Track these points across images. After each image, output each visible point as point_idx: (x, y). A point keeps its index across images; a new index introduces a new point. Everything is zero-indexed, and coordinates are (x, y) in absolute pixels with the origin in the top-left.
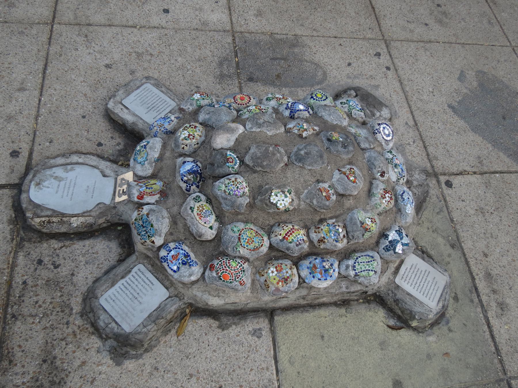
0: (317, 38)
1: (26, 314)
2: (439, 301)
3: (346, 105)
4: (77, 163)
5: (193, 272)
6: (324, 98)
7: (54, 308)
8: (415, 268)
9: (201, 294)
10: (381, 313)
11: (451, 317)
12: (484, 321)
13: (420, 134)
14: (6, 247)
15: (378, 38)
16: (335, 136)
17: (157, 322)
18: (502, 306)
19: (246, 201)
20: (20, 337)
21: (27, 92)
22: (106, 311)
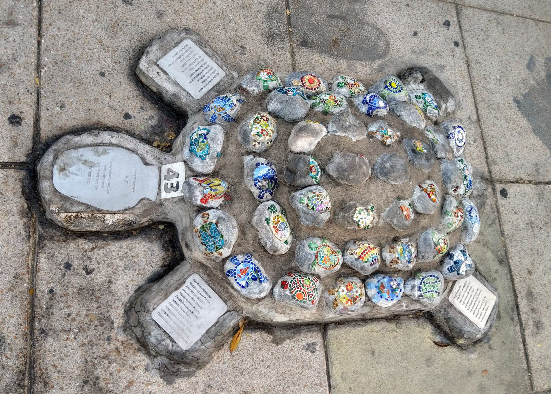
2: (487, 321)
3: (421, 100)
4: (110, 145)
5: (263, 288)
6: (399, 89)
7: (90, 321)
8: (468, 286)
9: (267, 311)
11: (492, 335)
12: (521, 340)
14: (25, 247)
16: (420, 146)
18: (538, 325)
19: (325, 216)
21: (20, 28)
22: (159, 326)
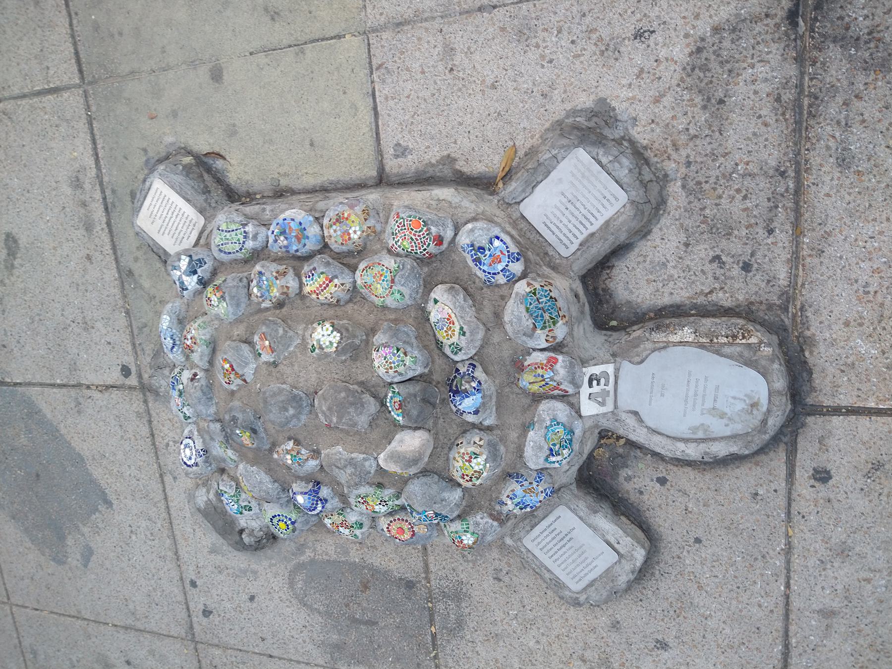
0: (301, 659)
1: (762, 178)
3: (243, 504)
4: (686, 441)
5: (468, 236)
6: (275, 520)
7: (714, 189)
9: (462, 204)
10: (232, 178)
12: (102, 162)
13: (158, 458)
14: (808, 295)
15: (203, 646)
16: (246, 438)
17: (536, 164)
18: (77, 184)
20: (766, 140)
21: (815, 607)
22: (617, 182)
